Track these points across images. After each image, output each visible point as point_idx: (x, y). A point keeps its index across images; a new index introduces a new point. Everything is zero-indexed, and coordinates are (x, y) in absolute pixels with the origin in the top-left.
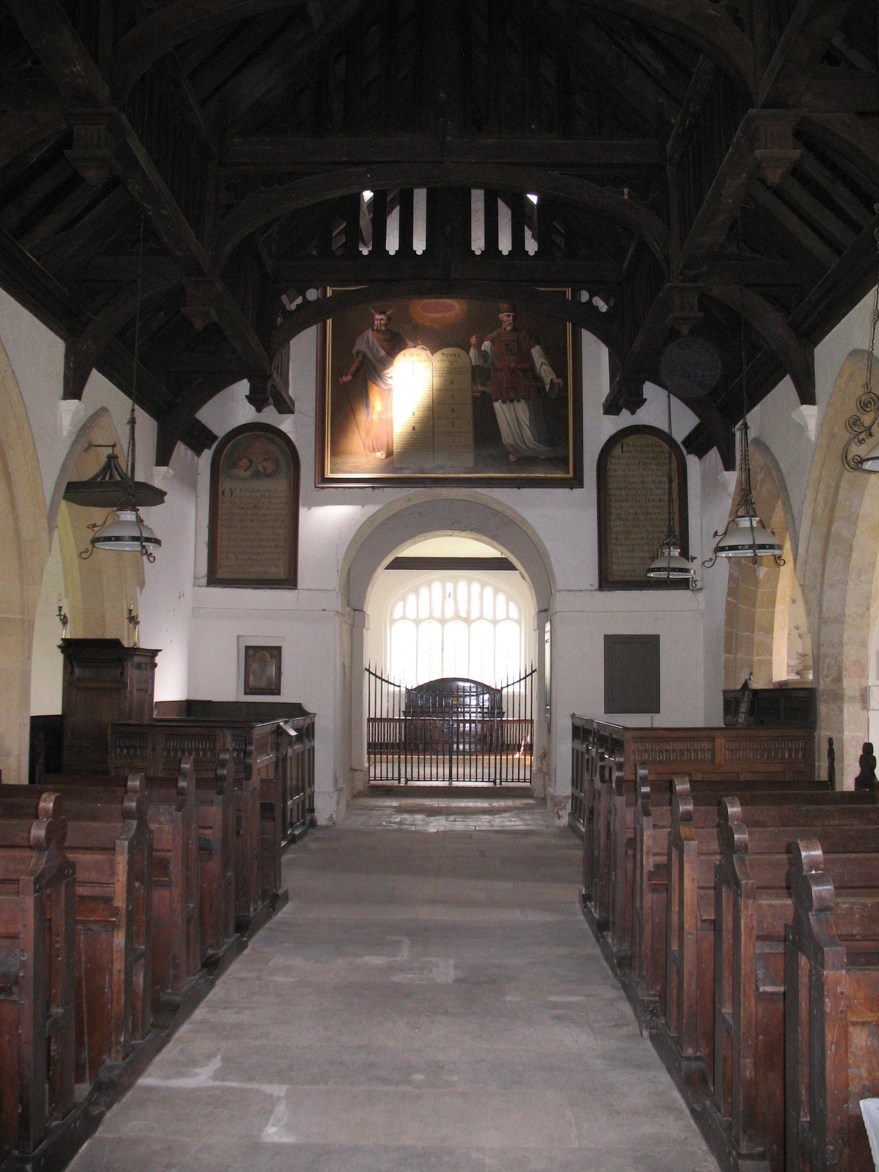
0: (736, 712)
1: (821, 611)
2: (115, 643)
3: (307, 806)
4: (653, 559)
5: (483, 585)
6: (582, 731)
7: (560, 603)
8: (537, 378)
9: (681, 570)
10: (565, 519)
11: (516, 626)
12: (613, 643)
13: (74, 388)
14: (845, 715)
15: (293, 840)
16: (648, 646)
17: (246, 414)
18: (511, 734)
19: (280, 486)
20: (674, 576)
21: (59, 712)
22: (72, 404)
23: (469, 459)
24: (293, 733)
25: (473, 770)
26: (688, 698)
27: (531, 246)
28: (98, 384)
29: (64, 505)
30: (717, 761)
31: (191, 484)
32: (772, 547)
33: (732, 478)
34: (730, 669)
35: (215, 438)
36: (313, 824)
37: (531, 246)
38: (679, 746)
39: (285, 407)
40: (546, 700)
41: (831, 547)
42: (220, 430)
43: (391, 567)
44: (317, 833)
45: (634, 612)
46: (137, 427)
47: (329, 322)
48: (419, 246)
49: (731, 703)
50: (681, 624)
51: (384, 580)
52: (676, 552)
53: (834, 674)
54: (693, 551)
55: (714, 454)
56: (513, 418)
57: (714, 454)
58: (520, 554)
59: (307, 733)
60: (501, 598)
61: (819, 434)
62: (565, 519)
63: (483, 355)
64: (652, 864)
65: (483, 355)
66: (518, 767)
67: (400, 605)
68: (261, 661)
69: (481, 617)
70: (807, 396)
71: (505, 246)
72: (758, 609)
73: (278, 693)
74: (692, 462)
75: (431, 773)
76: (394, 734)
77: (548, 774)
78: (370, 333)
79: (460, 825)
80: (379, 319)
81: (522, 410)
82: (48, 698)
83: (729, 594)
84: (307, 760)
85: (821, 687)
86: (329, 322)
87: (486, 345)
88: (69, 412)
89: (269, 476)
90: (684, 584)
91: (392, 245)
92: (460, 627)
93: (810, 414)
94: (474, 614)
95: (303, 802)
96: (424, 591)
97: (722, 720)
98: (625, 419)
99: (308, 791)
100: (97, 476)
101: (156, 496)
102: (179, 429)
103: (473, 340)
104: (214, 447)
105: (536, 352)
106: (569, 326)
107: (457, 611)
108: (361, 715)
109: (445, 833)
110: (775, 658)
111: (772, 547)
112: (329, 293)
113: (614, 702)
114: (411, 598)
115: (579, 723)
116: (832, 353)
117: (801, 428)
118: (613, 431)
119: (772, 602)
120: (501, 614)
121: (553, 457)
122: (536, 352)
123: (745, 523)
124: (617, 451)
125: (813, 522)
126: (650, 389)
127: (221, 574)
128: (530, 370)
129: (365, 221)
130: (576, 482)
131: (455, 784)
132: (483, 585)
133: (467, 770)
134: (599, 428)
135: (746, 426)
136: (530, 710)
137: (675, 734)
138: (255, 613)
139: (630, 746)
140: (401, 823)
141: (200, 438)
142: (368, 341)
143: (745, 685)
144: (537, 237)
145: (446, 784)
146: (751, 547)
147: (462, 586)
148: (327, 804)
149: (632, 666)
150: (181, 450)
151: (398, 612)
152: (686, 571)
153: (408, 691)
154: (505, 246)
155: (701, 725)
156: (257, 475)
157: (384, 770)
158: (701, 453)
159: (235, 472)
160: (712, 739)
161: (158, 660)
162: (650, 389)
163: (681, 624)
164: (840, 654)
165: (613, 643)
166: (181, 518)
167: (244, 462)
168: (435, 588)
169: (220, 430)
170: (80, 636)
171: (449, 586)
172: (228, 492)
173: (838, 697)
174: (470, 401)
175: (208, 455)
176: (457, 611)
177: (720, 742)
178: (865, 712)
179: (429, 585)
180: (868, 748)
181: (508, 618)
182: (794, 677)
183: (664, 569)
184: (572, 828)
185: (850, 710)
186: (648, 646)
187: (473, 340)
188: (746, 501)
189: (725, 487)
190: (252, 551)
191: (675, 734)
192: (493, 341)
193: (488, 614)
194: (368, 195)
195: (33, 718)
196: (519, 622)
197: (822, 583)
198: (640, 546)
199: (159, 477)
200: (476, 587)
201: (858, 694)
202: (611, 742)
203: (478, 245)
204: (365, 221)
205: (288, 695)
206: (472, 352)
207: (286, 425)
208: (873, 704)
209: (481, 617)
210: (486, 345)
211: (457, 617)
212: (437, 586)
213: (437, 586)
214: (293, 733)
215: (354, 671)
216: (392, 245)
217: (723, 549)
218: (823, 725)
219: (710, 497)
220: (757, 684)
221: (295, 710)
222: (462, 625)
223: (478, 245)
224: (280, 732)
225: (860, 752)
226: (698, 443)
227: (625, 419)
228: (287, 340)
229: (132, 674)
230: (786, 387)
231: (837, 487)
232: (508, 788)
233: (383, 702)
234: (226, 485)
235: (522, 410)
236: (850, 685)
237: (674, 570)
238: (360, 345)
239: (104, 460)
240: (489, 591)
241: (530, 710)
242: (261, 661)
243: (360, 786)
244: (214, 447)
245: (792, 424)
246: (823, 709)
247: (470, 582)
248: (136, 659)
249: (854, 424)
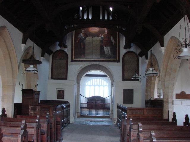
0: (148, 104)
1: (164, 86)
2: (32, 90)
3: (68, 120)
4: (133, 75)
5: (99, 79)
6: (119, 107)
7: (114, 84)
8: (112, 42)
9: (138, 78)
10: (117, 68)
11: (107, 87)
12: (125, 91)
13: (24, 42)
14: (169, 106)
15: (65, 126)
16: (132, 91)
17: (58, 48)
18: (106, 106)
19: (64, 61)
20: (137, 79)
21: (21, 103)
22: (24, 45)
23: (99, 57)
24: (65, 107)
25: (99, 113)
26: (138, 102)
27: (111, 18)
28: (30, 43)
29: (23, 64)
30: (145, 114)
31: (48, 61)
32: (156, 74)
33: (147, 61)
34: (147, 96)
35: (53, 52)
36: (69, 123)
37: (111, 18)
38: (137, 111)
39: (66, 47)
40: (112, 101)
41: (167, 74)
42: (54, 51)
43: (85, 76)
44: (70, 125)
45: (129, 85)
46: (34, 49)
47: (74, 31)
48: (90, 18)
49: (147, 102)
50: (138, 88)
51: (83, 78)
52: (137, 74)
53: (167, 98)
54: (140, 74)
55: (144, 57)
56: (107, 50)
57: (144, 57)
58: (108, 74)
59: (68, 107)
60: (105, 82)
61: (165, 52)
62: (117, 68)
63: (102, 38)
64: (133, 139)
65: (102, 38)
66: (107, 113)
67: (87, 83)
68: (61, 94)
69: (101, 85)
70: (162, 45)
71: (106, 18)
72: (152, 85)
73: (63, 99)
74: (140, 58)
75: (92, 113)
76: (85, 106)
77: (112, 114)
78: (81, 34)
79: (96, 124)
80: (83, 31)
81: (109, 48)
82: (18, 99)
83: (146, 82)
84: (68, 112)
85: (164, 100)
86: (74, 31)
87: (102, 36)
88: (23, 47)
89: (63, 59)
90: (138, 80)
91: (85, 18)
92: (97, 86)
93: (163, 49)
94: (100, 85)
95: (67, 119)
96: (91, 80)
97: (145, 106)
98: (127, 50)
99: (68, 117)
100: (29, 59)
101: (40, 63)
102: (46, 51)
103: (100, 35)
104: (53, 54)
105: (111, 38)
106: (118, 33)
107: (97, 84)
108: (79, 102)
109: (93, 125)
110: (155, 94)
111: (156, 74)
112: (74, 26)
113: (125, 102)
114: (89, 82)
115: (118, 105)
116: (167, 38)
117: (161, 51)
118: (125, 52)
119: (154, 84)
120: (105, 85)
121: (114, 57)
122: (111, 38)
123: (151, 69)
124: (126, 56)
125: (163, 69)
126: (132, 44)
127: (54, 77)
128: (111, 41)
129: (81, 13)
130: (119, 61)
131: (96, 115)
132: (99, 79)
133: (99, 113)
134: (123, 52)
135: (151, 51)
136: (110, 102)
137: (137, 109)
138: (59, 84)
139: (128, 111)
140: (86, 123)
141: (50, 53)
142: (81, 35)
143: (150, 99)
144: (112, 17)
145: (94, 115)
146: (152, 74)
147: (94, 80)
148: (72, 120)
149: (128, 96)
150: (46, 54)
151: (87, 84)
152: (139, 78)
153: (88, 98)
154: (106, 18)
155: (141, 107)
156: (60, 59)
157: (83, 112)
158: (141, 56)
159: (56, 59)
160: (143, 110)
161: (40, 93)
162: (132, 44)
163: (138, 88)
164: (168, 94)
165: (125, 91)
166: (46, 67)
167: (58, 57)
168: (93, 80)
169: (54, 51)
170: (26, 88)
171: (96, 80)
172: (55, 62)
173: (167, 102)
174: (99, 46)
175: (51, 55)
176: (97, 84)
177: (145, 110)
178: (172, 105)
179: (92, 79)
180: (174, 113)
181: (106, 85)
182: (158, 98)
183: (134, 78)
184: (117, 124)
185: (170, 105)
186: (132, 91)
187: (100, 35)
188: (151, 65)
189: (146, 62)
190: (59, 73)
191: (137, 109)
192: (104, 35)
193: (103, 85)
194: (81, 8)
195: (15, 104)
196: (108, 86)
197: (165, 80)
198: (130, 74)
199: (42, 59)
200: (101, 80)
201: (171, 102)
202: (124, 110)
203: (101, 18)
204: (81, 13)
205: (65, 99)
206: (100, 37)
207: (66, 50)
208: (174, 104)
209: (101, 85)
210: (102, 36)
211: (97, 85)
212: (94, 80)
213: (94, 80)
214: (65, 107)
215: (78, 95)
216: (85, 18)
217: (147, 74)
218: (165, 108)
219: (143, 64)
220: (152, 99)
221: (67, 102)
222: (98, 87)
223: (101, 18)
224: (63, 107)
225: (184, 121)
226: (141, 55)
227: (127, 50)
228: (66, 34)
229: (36, 96)
230: (158, 44)
231: (168, 63)
232: (106, 116)
233: (82, 100)
234: (55, 61)
235: (109, 48)
236: (170, 100)
237: (137, 78)
238: (80, 36)
239: (30, 56)
240: (103, 81)
241: (110, 102)
242: (61, 94)
243: (79, 115)
244: (53, 54)
245: (160, 51)
246: (165, 104)
247: (95, 79)
248: (36, 93)
249: (176, 49)
